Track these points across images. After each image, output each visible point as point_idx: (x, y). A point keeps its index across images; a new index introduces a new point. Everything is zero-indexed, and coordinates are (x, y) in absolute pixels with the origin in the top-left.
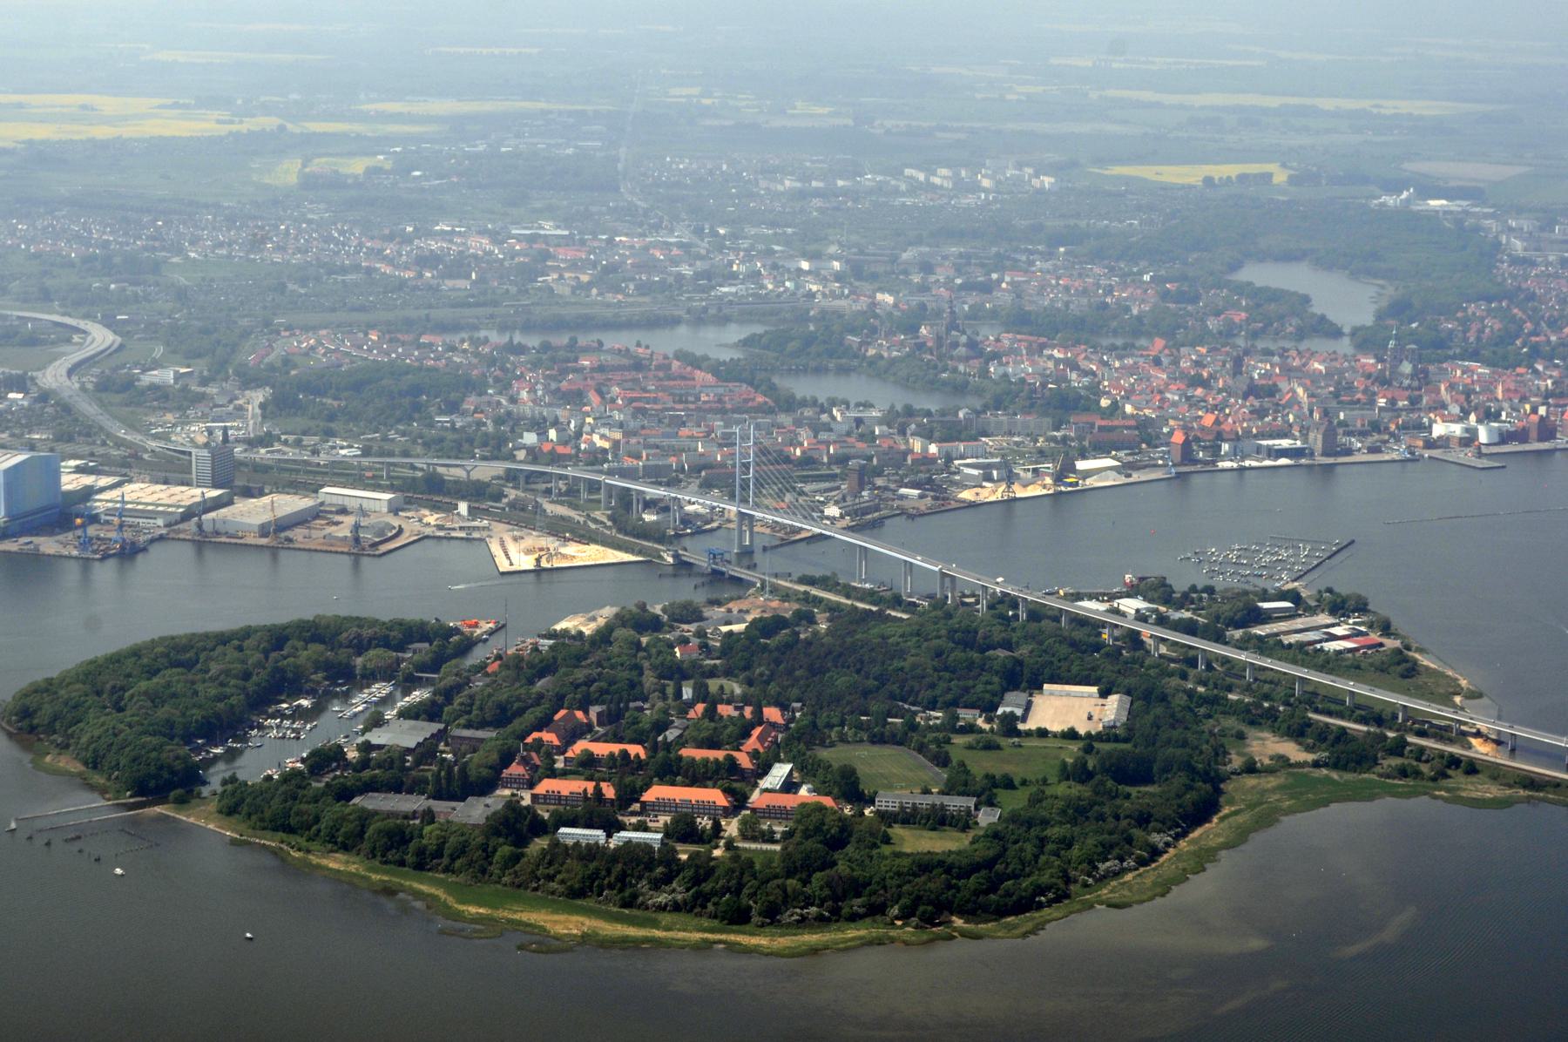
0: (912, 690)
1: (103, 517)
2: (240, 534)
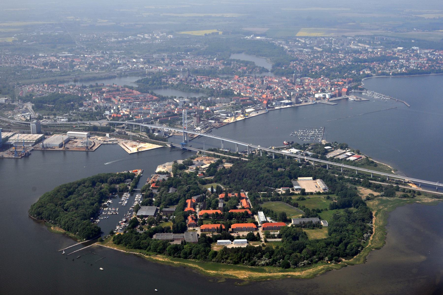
0: (270, 183)
1: (14, 145)
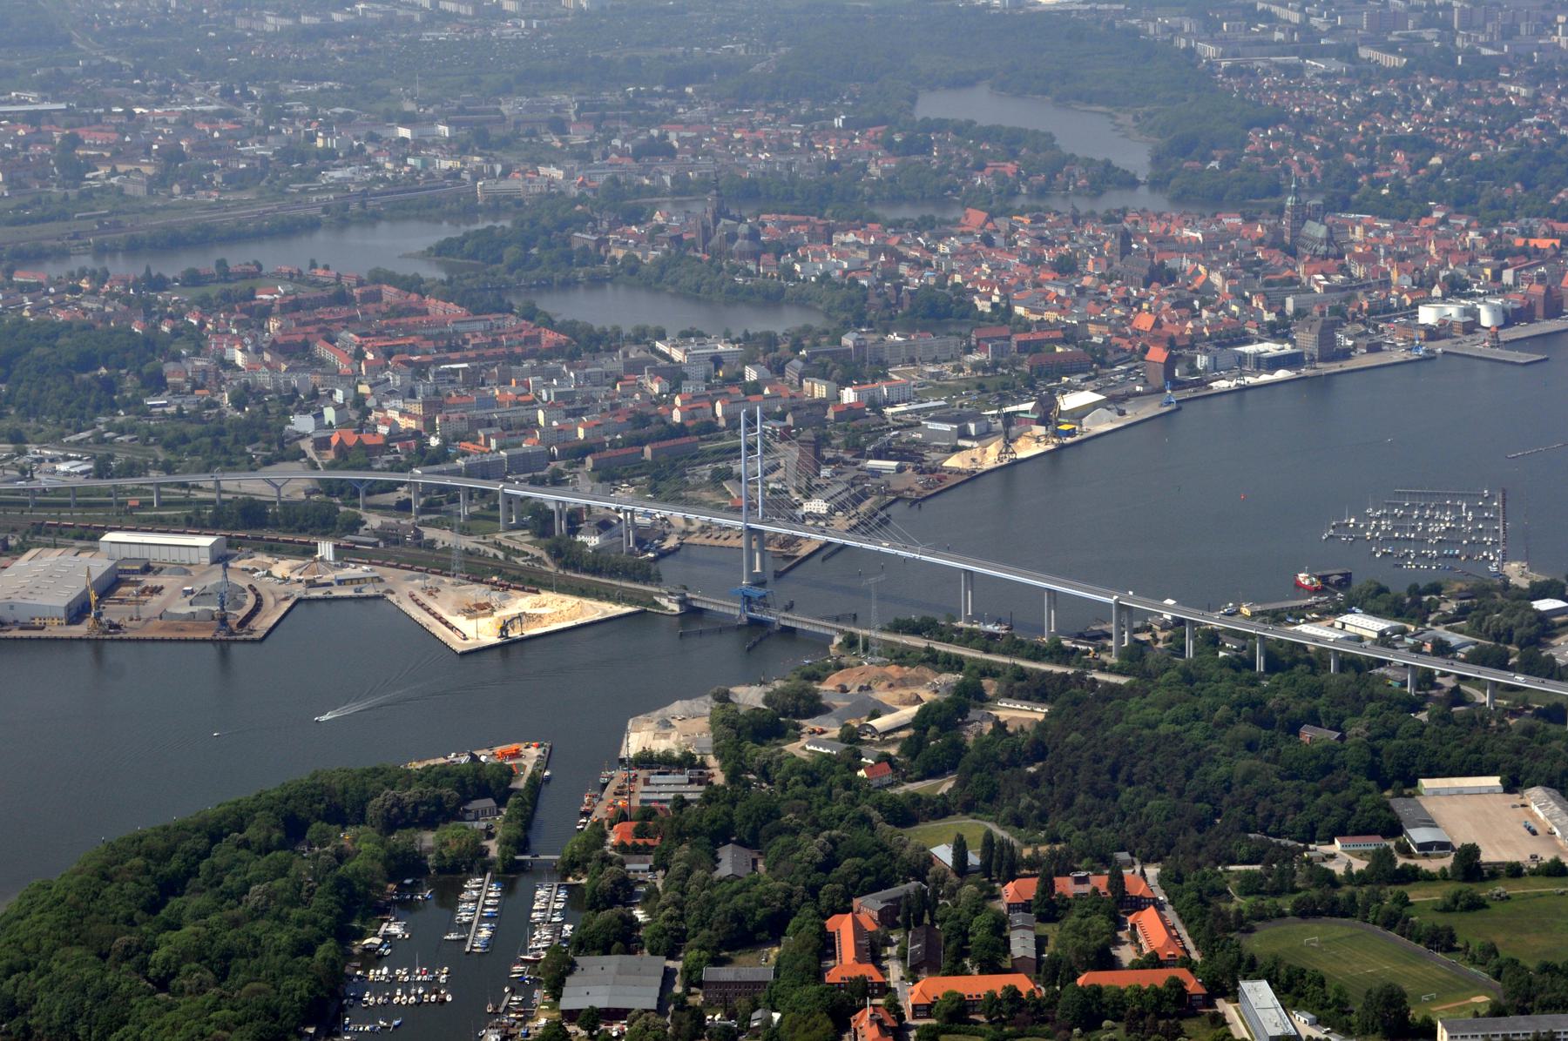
2: (37, 622)
